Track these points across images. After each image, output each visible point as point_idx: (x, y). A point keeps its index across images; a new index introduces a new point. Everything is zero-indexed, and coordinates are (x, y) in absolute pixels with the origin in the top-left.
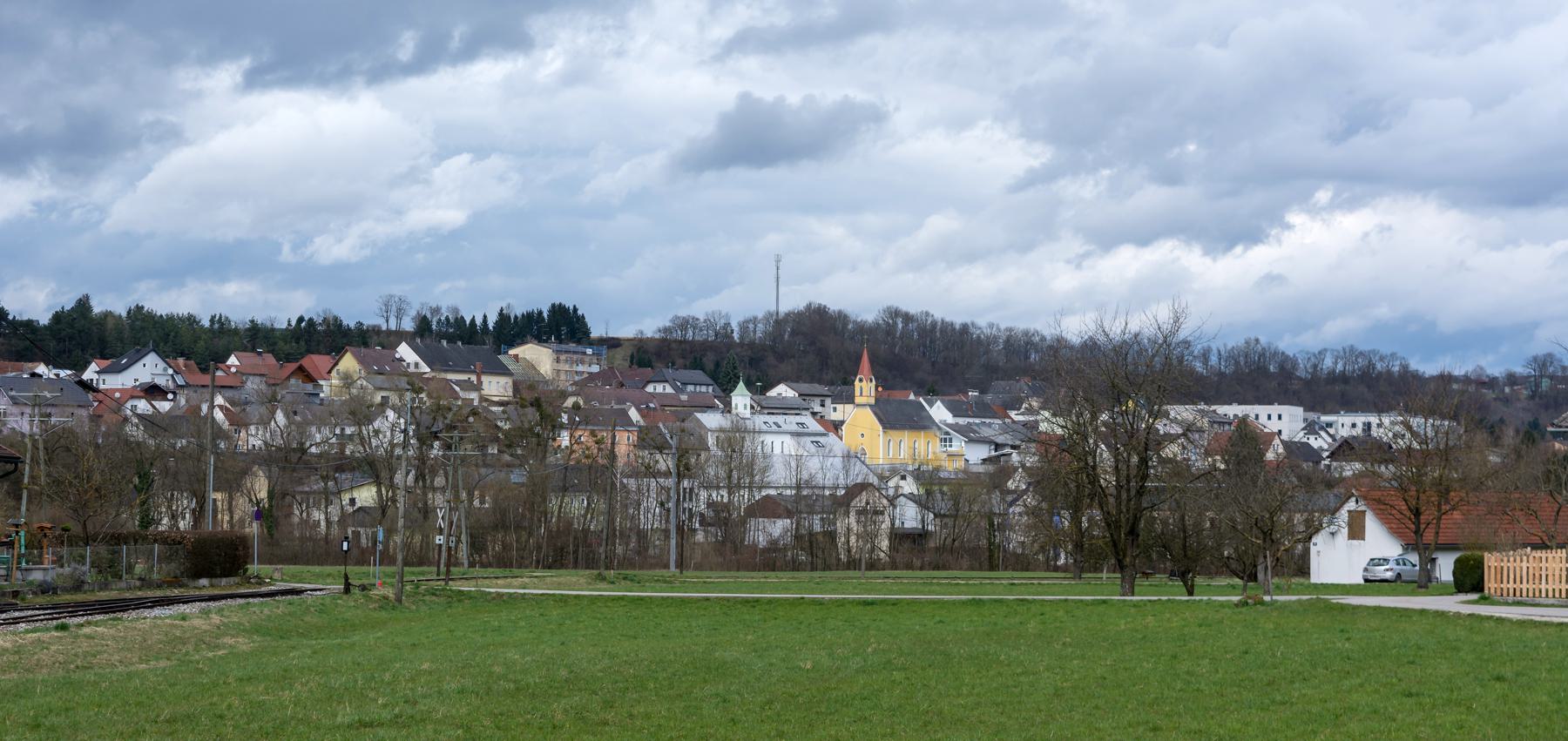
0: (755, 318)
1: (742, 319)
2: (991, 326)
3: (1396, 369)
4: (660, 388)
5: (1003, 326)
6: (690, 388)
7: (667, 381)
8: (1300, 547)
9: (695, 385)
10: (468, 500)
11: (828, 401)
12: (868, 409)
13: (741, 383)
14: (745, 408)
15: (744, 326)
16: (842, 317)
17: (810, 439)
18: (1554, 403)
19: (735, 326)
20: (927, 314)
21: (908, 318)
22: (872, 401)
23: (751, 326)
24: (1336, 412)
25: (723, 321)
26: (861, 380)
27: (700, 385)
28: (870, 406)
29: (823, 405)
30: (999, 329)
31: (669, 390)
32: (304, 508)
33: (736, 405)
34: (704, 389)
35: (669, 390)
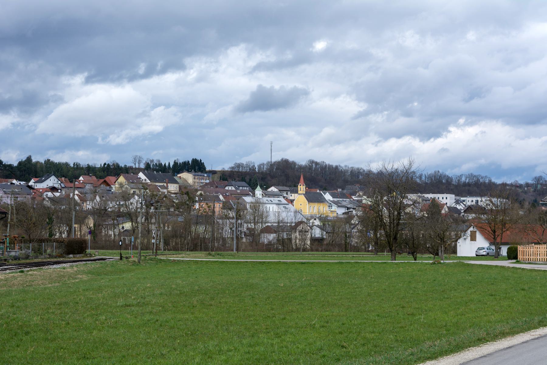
0: (264, 164)
2: (346, 166)
4: (230, 188)
5: (350, 166)
6: (241, 188)
7: (233, 186)
9: (243, 187)
11: (289, 193)
13: (259, 186)
14: (260, 195)
15: (259, 166)
16: (294, 163)
18: (542, 193)
20: (323, 162)
21: (317, 164)
22: (304, 193)
23: (262, 166)
26: (300, 185)
28: (304, 194)
29: (287, 194)
31: (233, 189)
34: (245, 188)
35: (233, 189)
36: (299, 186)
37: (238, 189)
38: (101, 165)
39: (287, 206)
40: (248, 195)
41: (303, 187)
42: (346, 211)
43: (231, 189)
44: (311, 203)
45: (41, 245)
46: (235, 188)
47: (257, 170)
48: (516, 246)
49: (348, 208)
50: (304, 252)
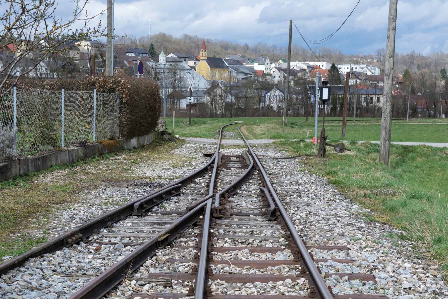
0: (144, 37)
1: (139, 37)
2: (216, 40)
3: (338, 53)
4: (130, 55)
5: (219, 40)
6: (141, 55)
7: (133, 52)
8: (236, 107)
9: (143, 53)
10: (347, 78)
11: (187, 59)
12: (205, 61)
13: (162, 52)
14: (164, 60)
15: (140, 40)
16: (170, 37)
17: (186, 71)
18: (447, 56)
19: (137, 39)
20: (196, 36)
21: (190, 38)
22: (206, 58)
23: (142, 40)
24: (342, 64)
25: (134, 38)
26: (202, 51)
27: (144, 54)
28: (206, 60)
29: (185, 61)
30: (218, 41)
31: (134, 55)
32: (9, 72)
33: (161, 60)
34: (145, 55)
35: (134, 55)
36: (201, 52)
37: (138, 56)
38: (7, 11)
39: (190, 71)
40: (150, 61)
41: (206, 53)
42: (244, 77)
43: (131, 55)
44: (214, 67)
45: (221, 204)
46: (135, 54)
47: (138, 43)
48: (261, 109)
49: (246, 74)
50: (381, 116)
